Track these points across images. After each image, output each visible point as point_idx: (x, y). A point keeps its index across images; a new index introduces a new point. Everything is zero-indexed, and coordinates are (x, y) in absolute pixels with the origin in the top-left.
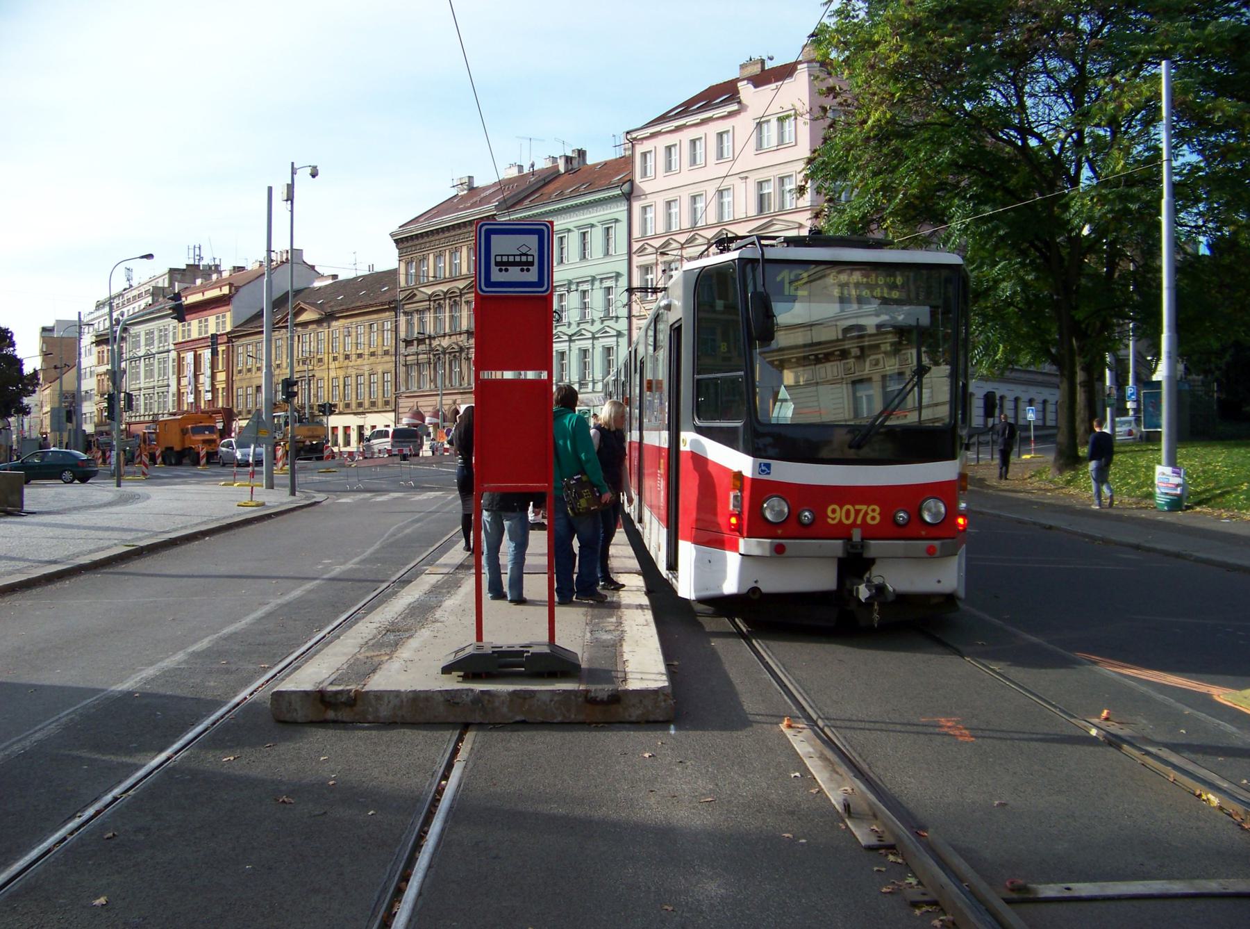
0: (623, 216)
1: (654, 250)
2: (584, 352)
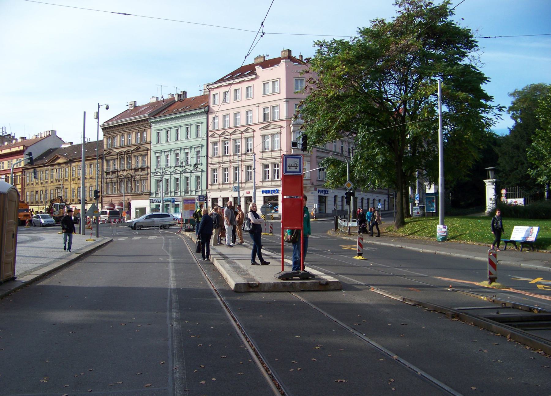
0: (205, 121)
1: (218, 136)
2: (187, 178)
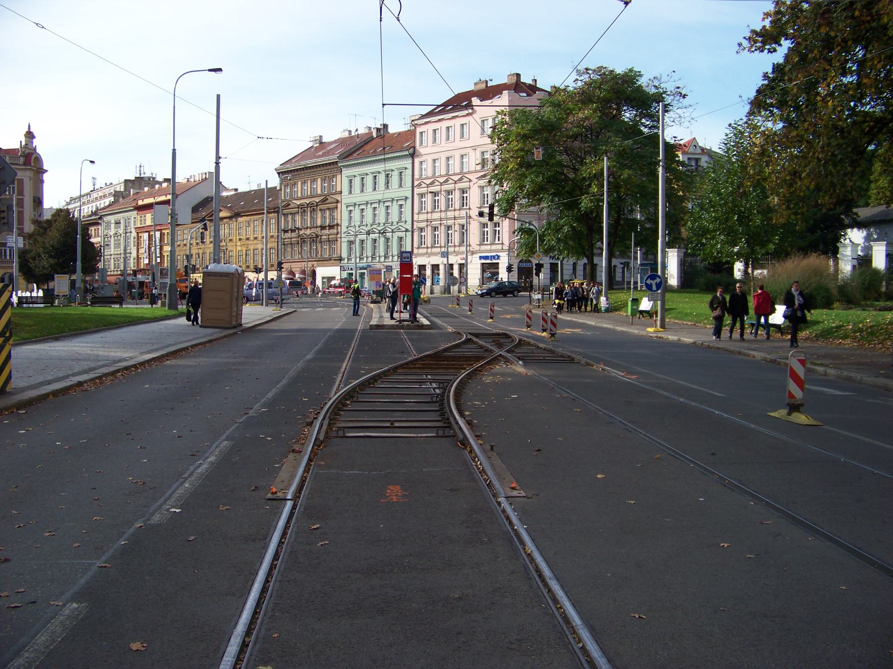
0: (410, 166)
